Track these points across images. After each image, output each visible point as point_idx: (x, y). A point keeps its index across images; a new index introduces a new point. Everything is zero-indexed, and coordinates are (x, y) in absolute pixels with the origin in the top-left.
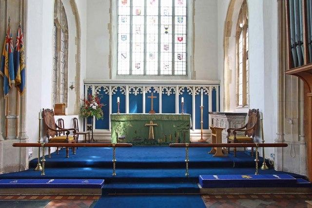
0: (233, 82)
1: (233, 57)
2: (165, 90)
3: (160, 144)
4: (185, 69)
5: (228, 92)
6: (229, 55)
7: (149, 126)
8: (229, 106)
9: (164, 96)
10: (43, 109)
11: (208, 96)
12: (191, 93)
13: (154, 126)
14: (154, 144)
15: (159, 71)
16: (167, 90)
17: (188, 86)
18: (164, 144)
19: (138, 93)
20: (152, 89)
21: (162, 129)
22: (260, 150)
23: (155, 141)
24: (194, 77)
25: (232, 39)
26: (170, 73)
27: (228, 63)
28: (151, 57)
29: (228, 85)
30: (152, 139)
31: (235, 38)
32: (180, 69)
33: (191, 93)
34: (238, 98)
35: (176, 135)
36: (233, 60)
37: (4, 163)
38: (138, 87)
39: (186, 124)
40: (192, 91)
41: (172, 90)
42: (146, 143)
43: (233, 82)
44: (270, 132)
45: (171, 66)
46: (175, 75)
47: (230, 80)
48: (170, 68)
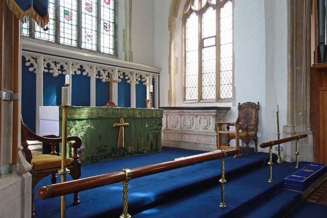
0: (179, 71)
1: (179, 43)
2: (48, 65)
3: (131, 154)
4: (74, 38)
5: (175, 83)
6: (176, 40)
7: (118, 127)
8: (175, 101)
9: (98, 81)
10: (239, 103)
11: (35, 75)
12: (35, 70)
13: (125, 127)
14: (124, 155)
15: (98, 45)
16: (53, 65)
17: (127, 71)
18: (136, 153)
19: (60, 72)
20: (81, 69)
21: (133, 132)
22: (274, 150)
23: (125, 150)
24: (131, 59)
25: (178, 20)
26: (94, 48)
27: (175, 50)
28: (66, 16)
29: (174, 74)
30: (123, 148)
31: (181, 21)
32: (107, 45)
33: (35, 70)
34: (185, 92)
35: (148, 137)
36: (180, 47)
37: (216, 150)
38: (104, 66)
39: (158, 123)
40: (35, 65)
41: (62, 67)
42: (113, 154)
43: (179, 71)
44: (268, 130)
45: (94, 38)
46: (81, 49)
47: (177, 69)
48: (94, 42)
